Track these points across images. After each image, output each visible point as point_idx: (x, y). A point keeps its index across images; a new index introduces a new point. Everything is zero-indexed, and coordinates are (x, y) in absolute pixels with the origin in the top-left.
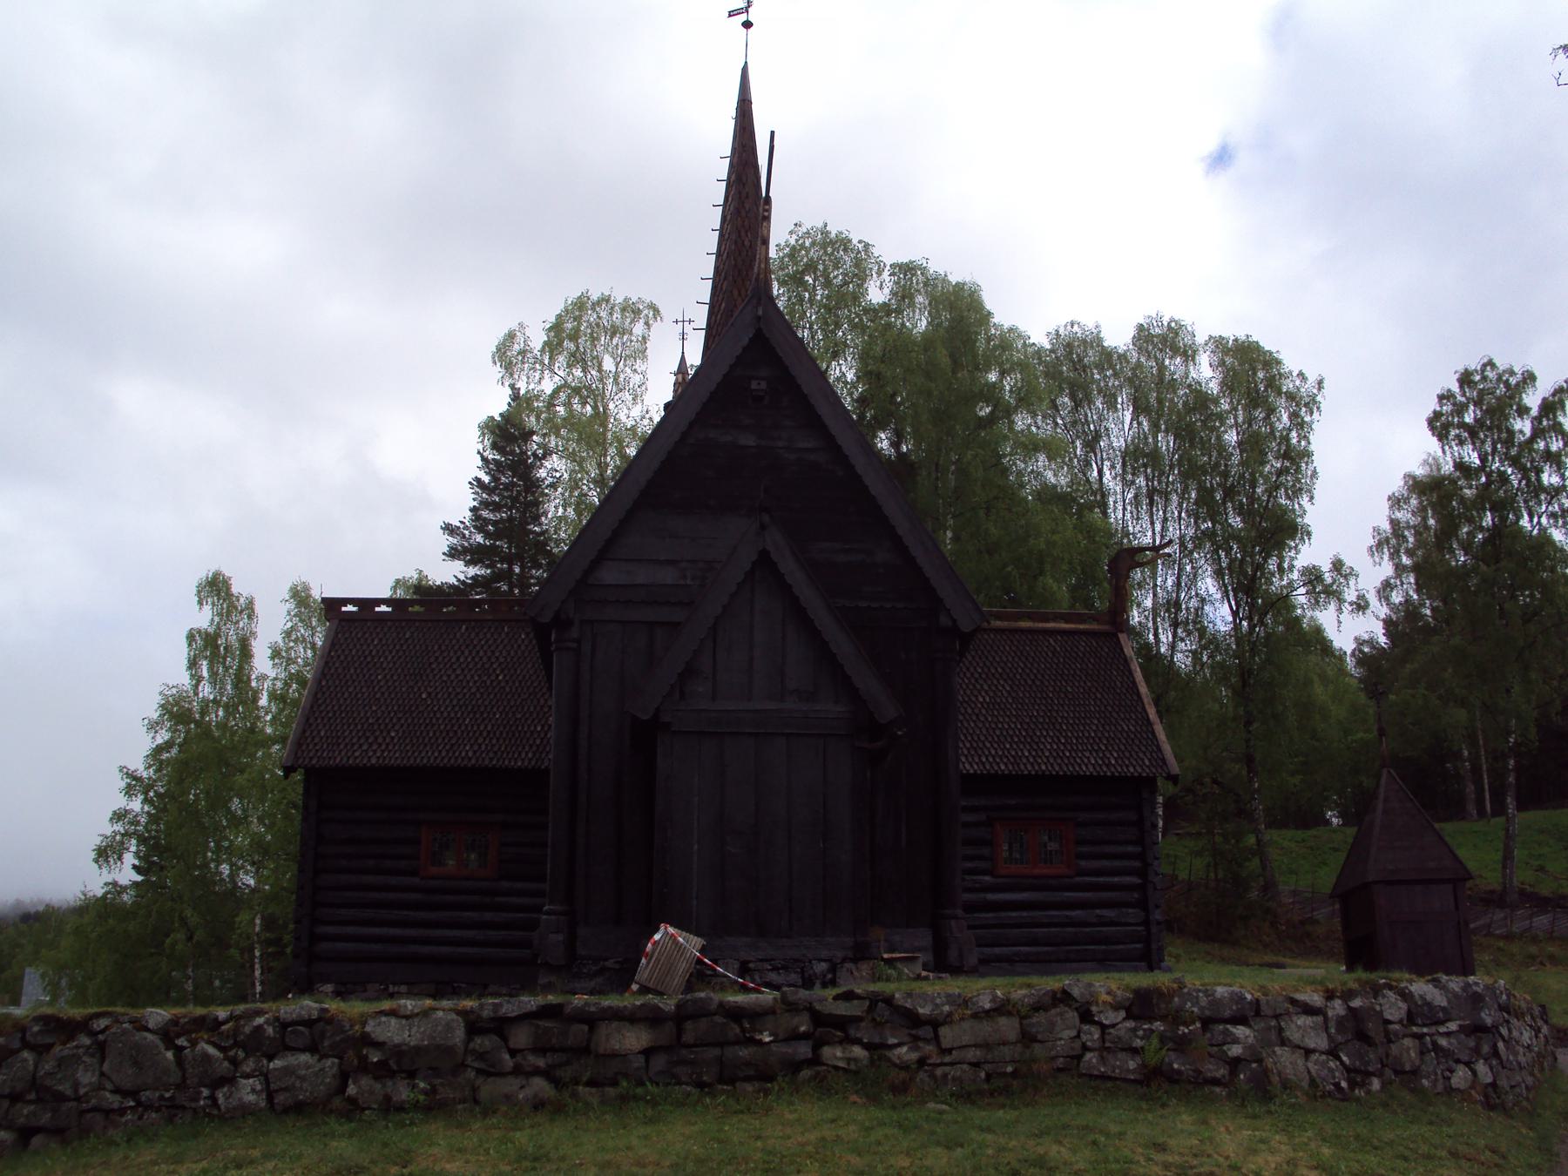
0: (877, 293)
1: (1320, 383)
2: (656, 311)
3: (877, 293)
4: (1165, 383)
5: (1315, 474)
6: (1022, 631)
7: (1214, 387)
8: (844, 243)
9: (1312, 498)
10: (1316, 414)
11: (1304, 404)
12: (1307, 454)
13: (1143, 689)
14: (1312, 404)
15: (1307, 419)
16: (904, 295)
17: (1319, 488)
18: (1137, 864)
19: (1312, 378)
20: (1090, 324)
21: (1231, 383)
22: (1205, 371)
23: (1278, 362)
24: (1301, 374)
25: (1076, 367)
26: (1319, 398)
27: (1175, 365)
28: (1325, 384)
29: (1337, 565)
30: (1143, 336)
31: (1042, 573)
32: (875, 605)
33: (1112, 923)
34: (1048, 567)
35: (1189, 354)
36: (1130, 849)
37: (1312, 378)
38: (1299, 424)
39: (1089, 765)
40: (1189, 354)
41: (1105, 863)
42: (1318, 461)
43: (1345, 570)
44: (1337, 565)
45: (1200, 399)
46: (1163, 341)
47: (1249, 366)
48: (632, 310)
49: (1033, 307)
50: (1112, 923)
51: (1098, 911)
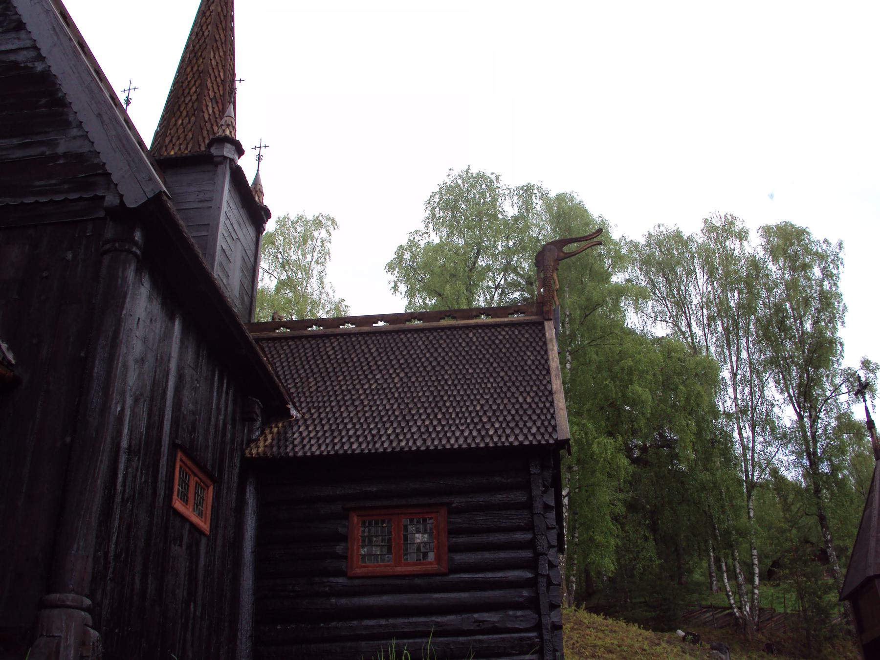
0: (510, 209)
1: (840, 245)
2: (333, 222)
3: (510, 209)
4: (729, 258)
5: (845, 309)
6: (443, 329)
7: (761, 253)
8: (481, 176)
9: (843, 323)
10: (841, 267)
11: (829, 261)
12: (838, 296)
13: (554, 362)
14: (837, 260)
15: (835, 272)
16: (527, 206)
17: (847, 317)
18: (527, 554)
19: (834, 242)
20: (672, 228)
21: (774, 252)
22: (755, 246)
23: (808, 233)
24: (826, 241)
25: (666, 258)
26: (840, 256)
27: (732, 244)
28: (844, 245)
29: (866, 364)
30: (709, 228)
31: (631, 382)
32: (43, 200)
33: (495, 630)
34: (635, 378)
35: (742, 236)
36: (519, 536)
37: (834, 242)
38: (827, 274)
39: (459, 438)
40: (742, 236)
41: (488, 555)
42: (846, 299)
43: (872, 366)
44: (866, 364)
45: (755, 265)
46: (726, 230)
47: (788, 241)
48: (318, 223)
49: (629, 218)
50: (495, 630)
51: (476, 616)
